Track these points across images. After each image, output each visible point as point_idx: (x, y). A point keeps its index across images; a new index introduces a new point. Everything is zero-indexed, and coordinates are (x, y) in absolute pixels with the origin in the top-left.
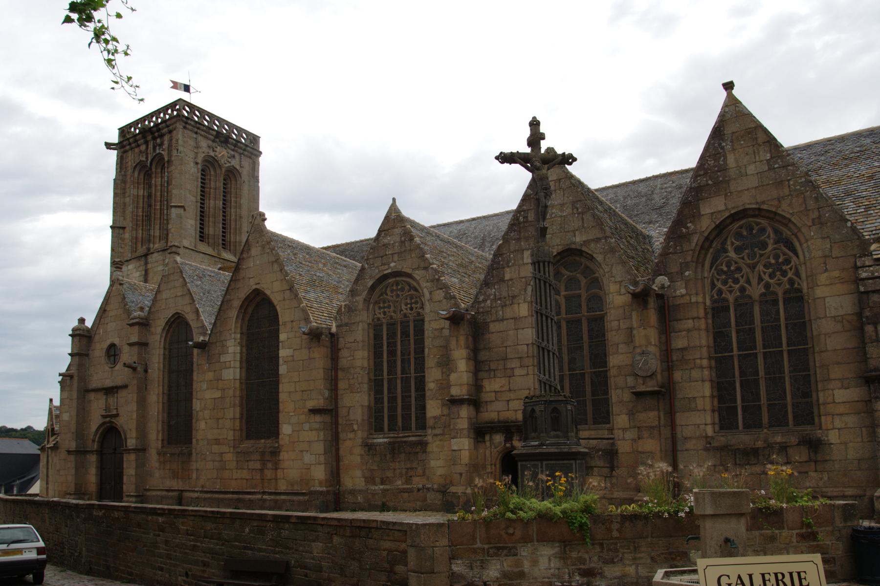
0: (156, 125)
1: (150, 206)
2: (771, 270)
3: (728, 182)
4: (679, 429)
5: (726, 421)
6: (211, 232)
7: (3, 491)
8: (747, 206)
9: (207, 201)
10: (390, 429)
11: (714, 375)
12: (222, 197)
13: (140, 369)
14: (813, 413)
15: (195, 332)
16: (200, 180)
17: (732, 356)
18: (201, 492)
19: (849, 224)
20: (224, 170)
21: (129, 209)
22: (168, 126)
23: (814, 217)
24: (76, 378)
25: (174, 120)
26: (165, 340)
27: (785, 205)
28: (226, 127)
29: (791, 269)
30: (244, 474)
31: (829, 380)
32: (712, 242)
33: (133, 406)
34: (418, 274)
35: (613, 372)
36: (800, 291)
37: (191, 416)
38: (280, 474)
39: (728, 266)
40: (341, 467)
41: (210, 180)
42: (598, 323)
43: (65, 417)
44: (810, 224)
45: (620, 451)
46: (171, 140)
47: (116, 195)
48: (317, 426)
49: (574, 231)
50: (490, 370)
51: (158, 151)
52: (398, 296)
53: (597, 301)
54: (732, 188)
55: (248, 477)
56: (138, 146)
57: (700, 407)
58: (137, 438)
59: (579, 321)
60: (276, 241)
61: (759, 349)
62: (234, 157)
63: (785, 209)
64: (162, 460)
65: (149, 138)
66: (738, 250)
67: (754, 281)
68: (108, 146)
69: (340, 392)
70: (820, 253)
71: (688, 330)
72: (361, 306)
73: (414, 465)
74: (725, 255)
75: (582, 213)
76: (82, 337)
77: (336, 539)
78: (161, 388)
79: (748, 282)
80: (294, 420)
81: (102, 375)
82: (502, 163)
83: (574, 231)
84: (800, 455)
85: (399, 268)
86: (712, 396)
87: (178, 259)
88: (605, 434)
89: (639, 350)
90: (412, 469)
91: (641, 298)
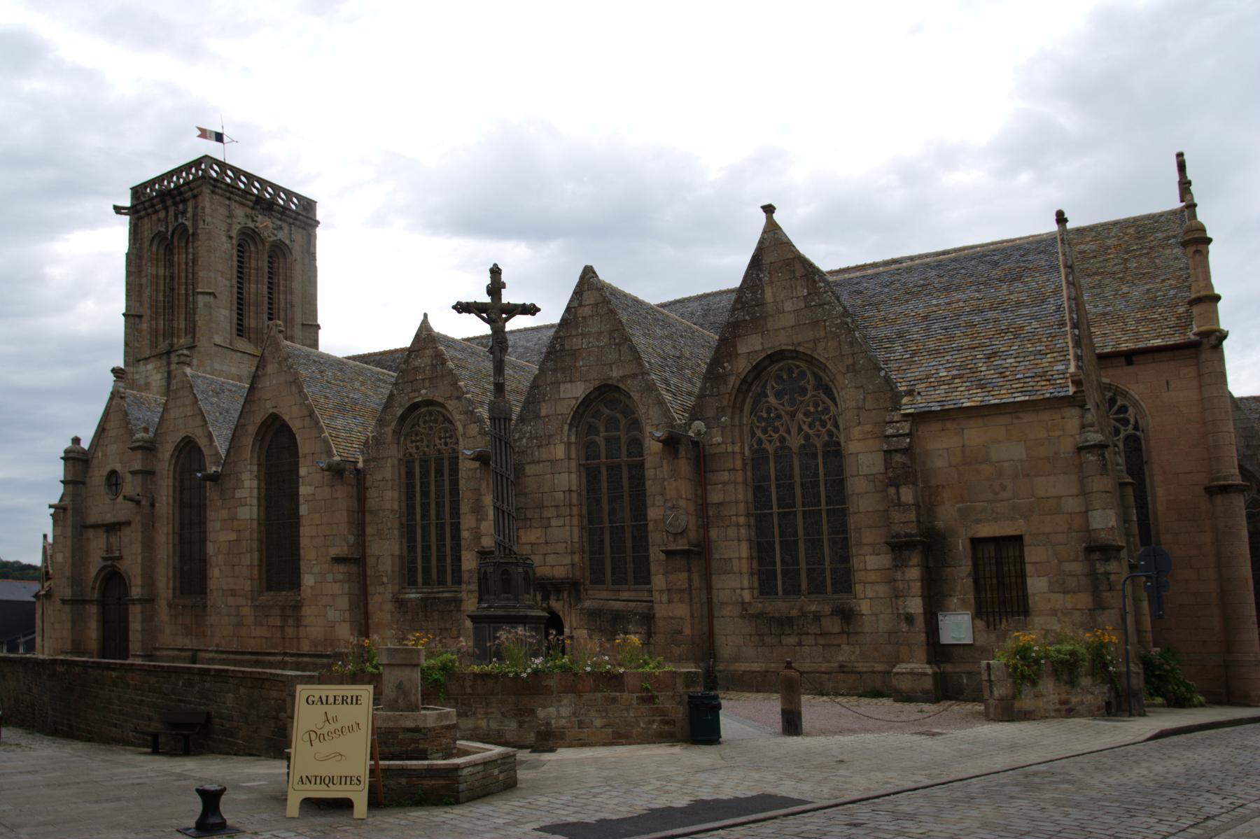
0: (178, 187)
1: (172, 290)
3: (765, 318)
4: (715, 592)
5: (766, 587)
6: (253, 325)
7: (5, 648)
9: (246, 285)
11: (753, 533)
12: (266, 280)
13: (146, 503)
15: (208, 460)
16: (235, 258)
17: (771, 514)
18: (216, 651)
19: (882, 373)
20: (267, 245)
21: (147, 293)
22: (191, 190)
24: (70, 512)
25: (199, 182)
27: (821, 346)
28: (270, 190)
31: (860, 544)
32: (751, 385)
33: (137, 548)
34: (451, 405)
35: (651, 527)
36: (839, 444)
37: (205, 561)
38: (302, 633)
39: (768, 412)
42: (638, 469)
43: (59, 558)
46: (196, 207)
47: (129, 274)
48: (341, 577)
49: (611, 365)
50: (526, 519)
52: (431, 428)
53: (636, 445)
54: (769, 326)
56: (156, 212)
57: (736, 569)
58: (143, 587)
59: (619, 467)
60: (298, 356)
61: (799, 508)
62: (281, 228)
63: (821, 354)
65: (169, 202)
66: (778, 395)
67: (794, 431)
68: (118, 210)
69: (368, 538)
70: (853, 404)
71: (724, 483)
72: (389, 438)
73: (448, 625)
75: (620, 344)
76: (76, 460)
77: (242, 690)
80: (316, 569)
81: (103, 508)
83: (611, 365)
84: (833, 625)
85: (430, 396)
86: (751, 558)
87: (188, 370)
89: (669, 504)
90: (446, 629)
91: (672, 443)
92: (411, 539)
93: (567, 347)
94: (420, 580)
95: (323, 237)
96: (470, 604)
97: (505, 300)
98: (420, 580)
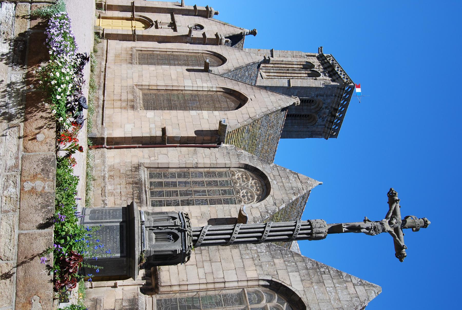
10: (151, 183)
41: (308, 106)
64: (128, 49)
94: (153, 180)
95: (320, 141)
98: (153, 180)
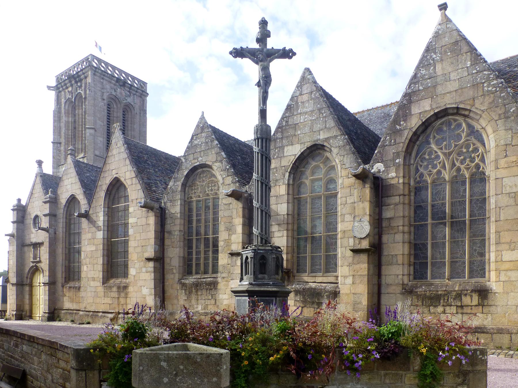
1: (75, 128)
2: (462, 157)
4: (383, 277)
8: (448, 106)
14: (485, 268)
17: (427, 225)
22: (84, 74)
23: (500, 112)
26: (66, 213)
29: (478, 156)
30: (108, 300)
32: (419, 136)
40: (166, 297)
44: (496, 118)
45: (341, 292)
51: (78, 91)
55: (110, 303)
56: (67, 88)
65: (73, 82)
68: (49, 88)
71: (396, 204)
74: (428, 146)
78: (64, 244)
79: (444, 167)
82: (235, 57)
88: (332, 279)
92: (190, 247)
93: (290, 123)
95: (150, 101)
96: (447, 151)
97: (269, 46)
